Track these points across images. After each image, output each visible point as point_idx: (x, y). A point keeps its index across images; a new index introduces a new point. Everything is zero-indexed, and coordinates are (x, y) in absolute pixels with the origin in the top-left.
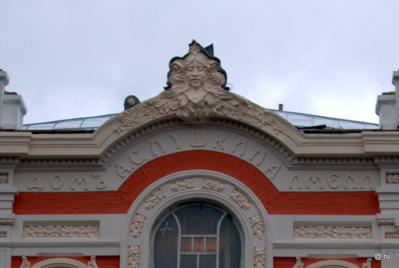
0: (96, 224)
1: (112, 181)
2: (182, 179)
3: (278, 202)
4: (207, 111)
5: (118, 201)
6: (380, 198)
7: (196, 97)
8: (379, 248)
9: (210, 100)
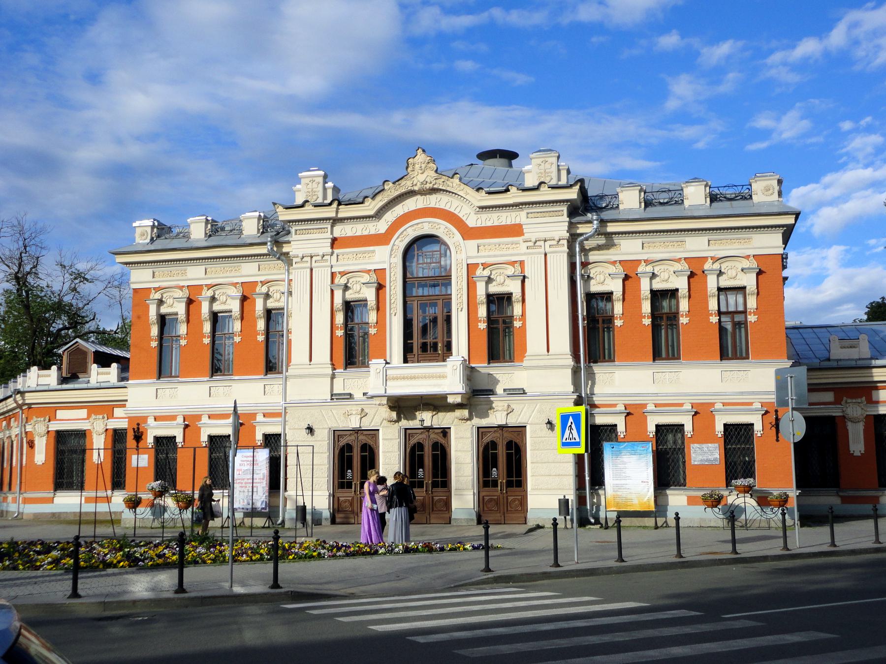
0: (373, 252)
1: (381, 226)
2: (417, 224)
3: (468, 233)
4: (428, 186)
6: (524, 227)
7: (421, 178)
8: (525, 254)
9: (428, 180)
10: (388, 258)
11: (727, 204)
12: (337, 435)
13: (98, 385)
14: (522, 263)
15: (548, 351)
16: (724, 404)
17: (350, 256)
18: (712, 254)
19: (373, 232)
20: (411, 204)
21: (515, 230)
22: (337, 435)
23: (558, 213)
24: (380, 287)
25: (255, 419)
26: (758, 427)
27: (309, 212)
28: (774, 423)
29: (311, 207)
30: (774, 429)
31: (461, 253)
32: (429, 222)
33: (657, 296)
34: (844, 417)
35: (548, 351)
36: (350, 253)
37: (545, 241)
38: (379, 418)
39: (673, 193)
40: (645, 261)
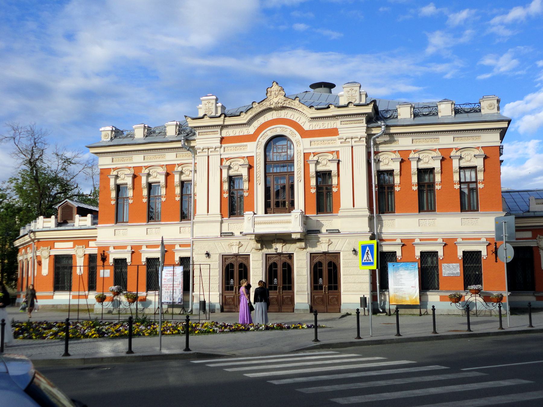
0: (246, 145)
1: (251, 130)
2: (273, 128)
3: (304, 134)
4: (280, 105)
5: (252, 138)
7: (276, 100)
8: (339, 147)
9: (280, 101)
10: (255, 149)
11: (466, 115)
12: (224, 258)
13: (79, 227)
14: (337, 152)
15: (354, 206)
16: (463, 239)
17: (232, 148)
18: (456, 146)
19: (246, 133)
20: (269, 116)
21: (334, 132)
22: (224, 258)
23: (360, 121)
24: (250, 167)
25: (174, 248)
26: (484, 253)
27: (207, 122)
28: (494, 251)
29: (208, 118)
30: (494, 254)
31: (300, 146)
32: (280, 127)
33: (421, 172)
34: (538, 247)
35: (354, 206)
36: (232, 146)
37: (352, 138)
38: (249, 247)
39: (431, 108)
40: (414, 151)
